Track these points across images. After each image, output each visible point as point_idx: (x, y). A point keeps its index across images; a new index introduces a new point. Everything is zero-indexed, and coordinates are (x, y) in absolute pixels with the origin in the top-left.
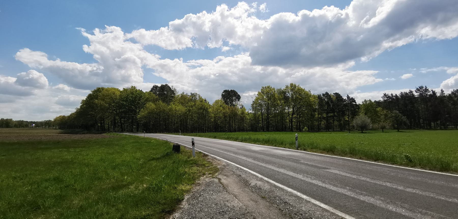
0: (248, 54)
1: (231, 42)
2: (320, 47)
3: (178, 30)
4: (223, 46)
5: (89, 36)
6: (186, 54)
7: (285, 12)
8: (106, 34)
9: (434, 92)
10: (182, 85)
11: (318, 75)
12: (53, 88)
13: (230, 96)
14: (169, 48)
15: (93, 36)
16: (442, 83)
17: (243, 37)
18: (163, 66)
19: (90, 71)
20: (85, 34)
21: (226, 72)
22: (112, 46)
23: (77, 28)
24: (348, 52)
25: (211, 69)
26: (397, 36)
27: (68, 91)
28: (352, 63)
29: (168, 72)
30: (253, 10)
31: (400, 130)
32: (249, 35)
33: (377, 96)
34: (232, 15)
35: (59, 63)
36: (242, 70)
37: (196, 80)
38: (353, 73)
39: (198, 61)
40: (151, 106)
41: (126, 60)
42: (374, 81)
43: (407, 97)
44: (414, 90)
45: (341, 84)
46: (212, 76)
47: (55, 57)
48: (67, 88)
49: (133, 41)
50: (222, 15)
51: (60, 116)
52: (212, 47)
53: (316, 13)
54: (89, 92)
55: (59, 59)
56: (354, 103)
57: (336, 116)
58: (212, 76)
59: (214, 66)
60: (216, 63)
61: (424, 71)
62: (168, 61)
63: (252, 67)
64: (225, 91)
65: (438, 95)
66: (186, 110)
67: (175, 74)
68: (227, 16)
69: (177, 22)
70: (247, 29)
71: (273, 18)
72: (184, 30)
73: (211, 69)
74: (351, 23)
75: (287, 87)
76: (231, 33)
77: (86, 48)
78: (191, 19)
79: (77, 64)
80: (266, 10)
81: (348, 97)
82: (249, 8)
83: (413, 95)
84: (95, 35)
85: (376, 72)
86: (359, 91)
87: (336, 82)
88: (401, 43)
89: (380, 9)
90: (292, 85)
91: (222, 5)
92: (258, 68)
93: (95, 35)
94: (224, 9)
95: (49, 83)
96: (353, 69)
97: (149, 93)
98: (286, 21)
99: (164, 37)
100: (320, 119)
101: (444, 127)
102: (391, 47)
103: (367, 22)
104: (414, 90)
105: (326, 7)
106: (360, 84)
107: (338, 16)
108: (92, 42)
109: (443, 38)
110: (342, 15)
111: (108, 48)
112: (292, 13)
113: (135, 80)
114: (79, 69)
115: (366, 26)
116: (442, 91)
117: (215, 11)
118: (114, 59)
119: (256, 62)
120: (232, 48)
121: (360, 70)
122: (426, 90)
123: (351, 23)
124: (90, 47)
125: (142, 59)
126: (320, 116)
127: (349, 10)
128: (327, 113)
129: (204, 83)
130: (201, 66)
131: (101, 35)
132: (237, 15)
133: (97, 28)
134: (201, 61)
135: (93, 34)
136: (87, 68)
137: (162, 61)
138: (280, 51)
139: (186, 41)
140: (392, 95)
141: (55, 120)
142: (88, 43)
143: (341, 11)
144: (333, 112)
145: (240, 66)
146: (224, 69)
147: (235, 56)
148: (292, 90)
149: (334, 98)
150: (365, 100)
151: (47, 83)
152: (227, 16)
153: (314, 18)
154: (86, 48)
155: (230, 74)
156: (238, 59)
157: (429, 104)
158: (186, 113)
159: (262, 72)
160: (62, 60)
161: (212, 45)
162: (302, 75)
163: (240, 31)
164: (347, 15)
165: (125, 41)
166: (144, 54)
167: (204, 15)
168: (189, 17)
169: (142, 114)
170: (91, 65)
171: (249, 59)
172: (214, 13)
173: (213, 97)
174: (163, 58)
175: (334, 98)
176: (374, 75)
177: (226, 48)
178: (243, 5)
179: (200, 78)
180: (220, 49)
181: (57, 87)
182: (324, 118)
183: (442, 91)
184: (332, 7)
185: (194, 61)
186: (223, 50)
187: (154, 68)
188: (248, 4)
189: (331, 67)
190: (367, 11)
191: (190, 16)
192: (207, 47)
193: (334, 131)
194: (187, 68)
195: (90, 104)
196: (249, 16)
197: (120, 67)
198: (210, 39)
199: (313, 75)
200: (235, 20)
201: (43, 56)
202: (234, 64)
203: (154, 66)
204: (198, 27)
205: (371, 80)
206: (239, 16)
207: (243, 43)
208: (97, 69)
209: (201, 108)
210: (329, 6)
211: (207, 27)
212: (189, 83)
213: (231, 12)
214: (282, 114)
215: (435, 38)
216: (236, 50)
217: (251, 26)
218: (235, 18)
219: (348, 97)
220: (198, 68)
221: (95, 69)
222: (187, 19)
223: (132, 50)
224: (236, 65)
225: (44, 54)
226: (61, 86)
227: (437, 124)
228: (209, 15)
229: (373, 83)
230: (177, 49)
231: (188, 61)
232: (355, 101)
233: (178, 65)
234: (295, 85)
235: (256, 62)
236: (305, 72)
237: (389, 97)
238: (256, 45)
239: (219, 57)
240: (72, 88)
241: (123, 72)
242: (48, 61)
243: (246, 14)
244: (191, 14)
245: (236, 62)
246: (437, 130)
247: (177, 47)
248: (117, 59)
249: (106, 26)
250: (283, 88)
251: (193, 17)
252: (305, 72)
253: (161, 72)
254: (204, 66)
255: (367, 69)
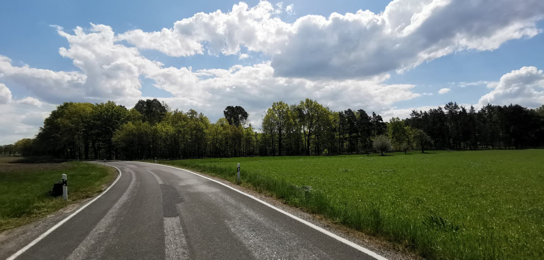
0: (269, 63)
1: (250, 49)
2: (353, 56)
3: (186, 32)
4: (242, 53)
5: (68, 36)
6: (195, 62)
7: (315, 14)
8: (90, 34)
9: (464, 110)
10: (191, 99)
11: (352, 88)
12: (18, 101)
13: (235, 114)
14: (174, 54)
15: (74, 36)
16: (480, 98)
17: (264, 43)
18: (167, 77)
19: (69, 82)
20: (63, 34)
21: (245, 84)
22: (98, 50)
23: (51, 26)
24: (383, 63)
25: (225, 81)
26: (434, 47)
27: (40, 106)
28: (388, 76)
29: (173, 83)
30: (278, 12)
31: (425, 151)
32: (270, 40)
33: (404, 114)
34: (251, 16)
35: (27, 70)
36: (264, 82)
37: (208, 93)
38: (388, 87)
39: (210, 71)
40: (130, 126)
41: (118, 68)
42: (411, 96)
43: (436, 114)
44: (443, 106)
45: (376, 99)
46: (228, 89)
47: (22, 62)
48: (37, 102)
49: (126, 44)
50: (240, 16)
51: (24, 139)
52: (227, 54)
53: (349, 17)
54: (54, 107)
55: (27, 65)
56: (381, 122)
57: (359, 137)
58: (228, 89)
59: (229, 77)
60: (232, 73)
61: (463, 85)
62: (172, 70)
63: (274, 78)
64: (229, 108)
65: (468, 111)
66: (175, 131)
67: (182, 86)
68: (246, 18)
69: (185, 22)
70: (269, 33)
71: (299, 22)
72: (193, 32)
73: (225, 81)
74: (388, 31)
75: (302, 103)
76: (250, 37)
77: (63, 52)
78: (202, 19)
79: (52, 71)
80: (293, 12)
81: (374, 114)
82: (273, 9)
83: (442, 112)
84: (76, 35)
85: (414, 86)
86: (396, 107)
87: (372, 97)
88: (440, 53)
89: (415, 16)
90: (307, 100)
91: (240, 3)
92: (282, 81)
93: (76, 35)
94: (243, 8)
95: (13, 98)
96: (389, 82)
97: (133, 111)
98: (316, 26)
99: (168, 40)
100: (342, 141)
101: (474, 147)
102: (429, 58)
103: (402, 28)
104: (443, 106)
105: (360, 11)
106: (392, 99)
107: (374, 22)
108: (72, 44)
109: (484, 49)
110: (378, 21)
111: (94, 52)
112: (323, 16)
113: (130, 93)
114: (54, 78)
115: (399, 36)
116: (472, 108)
117: (231, 11)
118: (101, 67)
119: (280, 73)
120: (251, 56)
121: (396, 84)
122: (456, 107)
123: (388, 31)
124: (69, 50)
125: (140, 67)
126: (342, 136)
127: (385, 16)
128: (350, 133)
129: (218, 97)
130: (214, 76)
131: (84, 36)
132: (258, 16)
133: (79, 26)
134: (213, 71)
135: (73, 33)
136: (65, 76)
137: (166, 70)
138: (306, 60)
139: (195, 46)
140: (421, 112)
141: (17, 144)
142: (67, 44)
143: (377, 17)
144: (357, 132)
145: (261, 77)
146: (242, 81)
147: (255, 65)
148: (307, 106)
149: (358, 116)
150: (393, 118)
151: (10, 96)
152: (246, 18)
153: (347, 23)
154: (63, 52)
155: (249, 87)
156: (258, 69)
157: (459, 122)
158: (175, 134)
159: (286, 85)
160: (32, 66)
161: (228, 52)
162: (332, 89)
163: (260, 36)
164: (383, 21)
165: (115, 43)
166: (141, 61)
167: (218, 15)
168: (199, 16)
169: (117, 136)
170: (70, 73)
171: (272, 70)
172: (230, 13)
173: (215, 115)
174: (167, 66)
175: (358, 116)
176: (411, 90)
177: (245, 56)
178: (265, 4)
179: (213, 91)
180: (237, 56)
181: (24, 100)
182: (346, 139)
183: (472, 108)
184: (368, 11)
185: (205, 70)
186: (240, 58)
187: (155, 79)
188: (272, 4)
189: (363, 80)
190: (403, 18)
191: (201, 15)
192: (221, 55)
193: (357, 154)
194: (197, 78)
195: (51, 124)
196: (272, 17)
197: (109, 76)
198: (226, 44)
199: (345, 88)
200: (255, 23)
201: (5, 61)
202: (254, 75)
203: (155, 76)
204: (209, 29)
205: (409, 96)
206: (260, 17)
207: (265, 50)
208: (78, 78)
209: (195, 129)
210: (364, 10)
211: (221, 30)
212: (199, 97)
213: (250, 12)
214: (298, 136)
215: (475, 49)
216: (256, 58)
217: (273, 30)
218: (255, 20)
219: (374, 114)
220: (210, 79)
221: (76, 78)
222: (196, 19)
223: (125, 55)
224: (257, 76)
225: (6, 58)
226: (30, 99)
227: (467, 144)
228: (224, 15)
229: (410, 98)
230: (184, 55)
231: (198, 71)
232: (381, 119)
233: (185, 75)
234: (311, 101)
235: (280, 73)
236: (336, 85)
237: (418, 114)
238: (279, 52)
239: (236, 66)
240: (45, 103)
241: (114, 82)
242: (12, 68)
243: (269, 15)
244: (202, 13)
245: (257, 72)
246: (466, 150)
247: (183, 53)
248: (105, 67)
249: (91, 23)
250: (298, 104)
251: (204, 17)
252: (336, 85)
253: (164, 83)
254: (217, 77)
255: (403, 83)
